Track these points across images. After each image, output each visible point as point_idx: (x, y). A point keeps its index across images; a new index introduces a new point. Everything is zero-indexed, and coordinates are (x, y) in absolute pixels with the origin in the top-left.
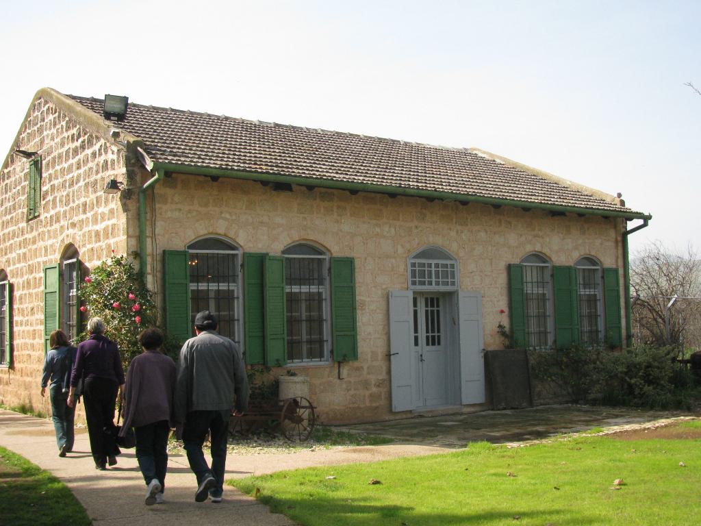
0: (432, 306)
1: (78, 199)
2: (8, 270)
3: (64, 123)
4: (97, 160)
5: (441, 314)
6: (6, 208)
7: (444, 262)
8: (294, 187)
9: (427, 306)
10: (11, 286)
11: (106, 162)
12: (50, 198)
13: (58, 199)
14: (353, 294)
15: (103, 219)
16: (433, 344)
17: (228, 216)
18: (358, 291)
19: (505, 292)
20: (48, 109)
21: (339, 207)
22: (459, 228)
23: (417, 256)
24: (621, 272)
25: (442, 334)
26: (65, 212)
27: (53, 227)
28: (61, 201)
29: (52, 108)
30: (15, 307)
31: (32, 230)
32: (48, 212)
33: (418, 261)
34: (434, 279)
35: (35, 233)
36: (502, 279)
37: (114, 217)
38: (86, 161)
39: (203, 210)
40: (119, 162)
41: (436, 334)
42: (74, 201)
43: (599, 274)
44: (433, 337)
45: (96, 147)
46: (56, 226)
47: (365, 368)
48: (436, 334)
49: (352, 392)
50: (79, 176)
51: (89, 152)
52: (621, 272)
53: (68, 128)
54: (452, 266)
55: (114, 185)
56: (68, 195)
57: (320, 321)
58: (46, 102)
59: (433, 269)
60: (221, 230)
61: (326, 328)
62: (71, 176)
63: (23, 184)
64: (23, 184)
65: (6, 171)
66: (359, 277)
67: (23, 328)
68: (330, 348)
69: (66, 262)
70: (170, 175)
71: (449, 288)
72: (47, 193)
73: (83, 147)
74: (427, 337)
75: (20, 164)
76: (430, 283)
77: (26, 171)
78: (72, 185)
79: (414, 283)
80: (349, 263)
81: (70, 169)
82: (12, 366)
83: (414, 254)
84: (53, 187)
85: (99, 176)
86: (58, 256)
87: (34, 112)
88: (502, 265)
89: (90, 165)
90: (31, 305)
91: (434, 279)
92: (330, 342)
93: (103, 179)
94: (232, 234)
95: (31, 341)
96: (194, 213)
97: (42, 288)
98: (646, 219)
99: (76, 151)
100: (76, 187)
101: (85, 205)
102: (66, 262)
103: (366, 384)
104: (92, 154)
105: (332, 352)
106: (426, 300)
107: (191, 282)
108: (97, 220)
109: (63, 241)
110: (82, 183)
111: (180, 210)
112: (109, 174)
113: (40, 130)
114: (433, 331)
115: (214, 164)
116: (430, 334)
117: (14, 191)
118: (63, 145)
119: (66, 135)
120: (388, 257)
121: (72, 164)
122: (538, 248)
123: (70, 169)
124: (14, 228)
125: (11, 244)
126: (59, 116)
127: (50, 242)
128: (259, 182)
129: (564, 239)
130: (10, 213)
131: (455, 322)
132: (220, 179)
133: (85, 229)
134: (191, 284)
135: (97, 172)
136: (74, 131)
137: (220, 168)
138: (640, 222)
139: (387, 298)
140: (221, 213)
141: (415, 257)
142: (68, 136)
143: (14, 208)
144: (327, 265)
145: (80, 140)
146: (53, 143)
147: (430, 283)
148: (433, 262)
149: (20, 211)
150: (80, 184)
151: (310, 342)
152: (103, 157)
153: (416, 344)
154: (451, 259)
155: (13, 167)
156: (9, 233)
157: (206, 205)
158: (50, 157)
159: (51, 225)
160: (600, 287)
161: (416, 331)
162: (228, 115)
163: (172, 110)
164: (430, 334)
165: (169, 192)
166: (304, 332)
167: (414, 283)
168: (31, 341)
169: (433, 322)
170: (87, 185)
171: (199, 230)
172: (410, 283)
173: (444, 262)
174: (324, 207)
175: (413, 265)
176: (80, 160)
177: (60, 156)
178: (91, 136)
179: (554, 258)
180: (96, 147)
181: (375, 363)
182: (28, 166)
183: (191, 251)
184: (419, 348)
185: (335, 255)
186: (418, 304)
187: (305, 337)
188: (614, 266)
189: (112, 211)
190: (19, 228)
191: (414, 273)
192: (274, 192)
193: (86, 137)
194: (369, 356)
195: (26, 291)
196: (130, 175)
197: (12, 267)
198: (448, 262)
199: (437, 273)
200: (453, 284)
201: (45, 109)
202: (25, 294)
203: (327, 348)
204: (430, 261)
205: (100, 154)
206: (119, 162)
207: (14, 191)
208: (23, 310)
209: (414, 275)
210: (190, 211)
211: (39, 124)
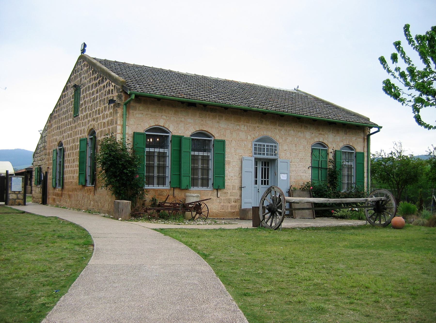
1: (96, 107)
2: (63, 141)
3: (91, 72)
4: (105, 89)
6: (63, 112)
9: (262, 166)
11: (109, 90)
12: (84, 107)
13: (87, 107)
16: (265, 184)
17: (165, 118)
20: (84, 65)
22: (280, 128)
23: (258, 141)
24: (366, 154)
25: (269, 180)
26: (90, 114)
27: (85, 121)
28: (88, 108)
29: (86, 64)
32: (82, 113)
33: (257, 143)
35: (76, 124)
37: (112, 116)
40: (114, 90)
44: (265, 181)
45: (105, 83)
46: (86, 120)
47: (229, 193)
48: (267, 167)
49: (222, 204)
50: (97, 97)
51: (102, 85)
52: (366, 154)
53: (93, 74)
54: (276, 146)
56: (92, 105)
57: (208, 170)
58: (83, 61)
59: (266, 153)
62: (93, 96)
65: (64, 94)
66: (227, 150)
67: (70, 169)
72: (82, 104)
74: (262, 181)
75: (70, 90)
76: (264, 154)
78: (93, 101)
80: (223, 142)
85: (106, 97)
95: (73, 175)
98: (380, 128)
99: (96, 85)
100: (95, 102)
101: (99, 110)
104: (103, 86)
105: (213, 184)
107: (146, 148)
110: (98, 100)
111: (142, 114)
113: (80, 75)
114: (265, 178)
116: (263, 179)
117: (67, 103)
118: (90, 82)
119: (92, 77)
121: (94, 91)
124: (67, 121)
125: (65, 129)
128: (180, 102)
129: (335, 136)
134: (146, 148)
136: (96, 75)
138: (376, 129)
140: (162, 116)
141: (256, 141)
142: (93, 78)
143: (67, 112)
145: (98, 80)
148: (266, 144)
150: (97, 101)
151: (202, 179)
155: (67, 92)
156: (64, 124)
158: (84, 88)
164: (263, 179)
167: (255, 154)
168: (73, 175)
169: (265, 174)
170: (100, 101)
172: (253, 153)
175: (255, 145)
176: (98, 89)
180: (105, 83)
181: (234, 191)
183: (147, 133)
185: (216, 138)
186: (258, 165)
188: (362, 151)
190: (69, 121)
193: (101, 78)
197: (65, 140)
198: (274, 145)
201: (83, 65)
202: (71, 153)
204: (264, 144)
206: (114, 90)
207: (67, 103)
211: (80, 71)
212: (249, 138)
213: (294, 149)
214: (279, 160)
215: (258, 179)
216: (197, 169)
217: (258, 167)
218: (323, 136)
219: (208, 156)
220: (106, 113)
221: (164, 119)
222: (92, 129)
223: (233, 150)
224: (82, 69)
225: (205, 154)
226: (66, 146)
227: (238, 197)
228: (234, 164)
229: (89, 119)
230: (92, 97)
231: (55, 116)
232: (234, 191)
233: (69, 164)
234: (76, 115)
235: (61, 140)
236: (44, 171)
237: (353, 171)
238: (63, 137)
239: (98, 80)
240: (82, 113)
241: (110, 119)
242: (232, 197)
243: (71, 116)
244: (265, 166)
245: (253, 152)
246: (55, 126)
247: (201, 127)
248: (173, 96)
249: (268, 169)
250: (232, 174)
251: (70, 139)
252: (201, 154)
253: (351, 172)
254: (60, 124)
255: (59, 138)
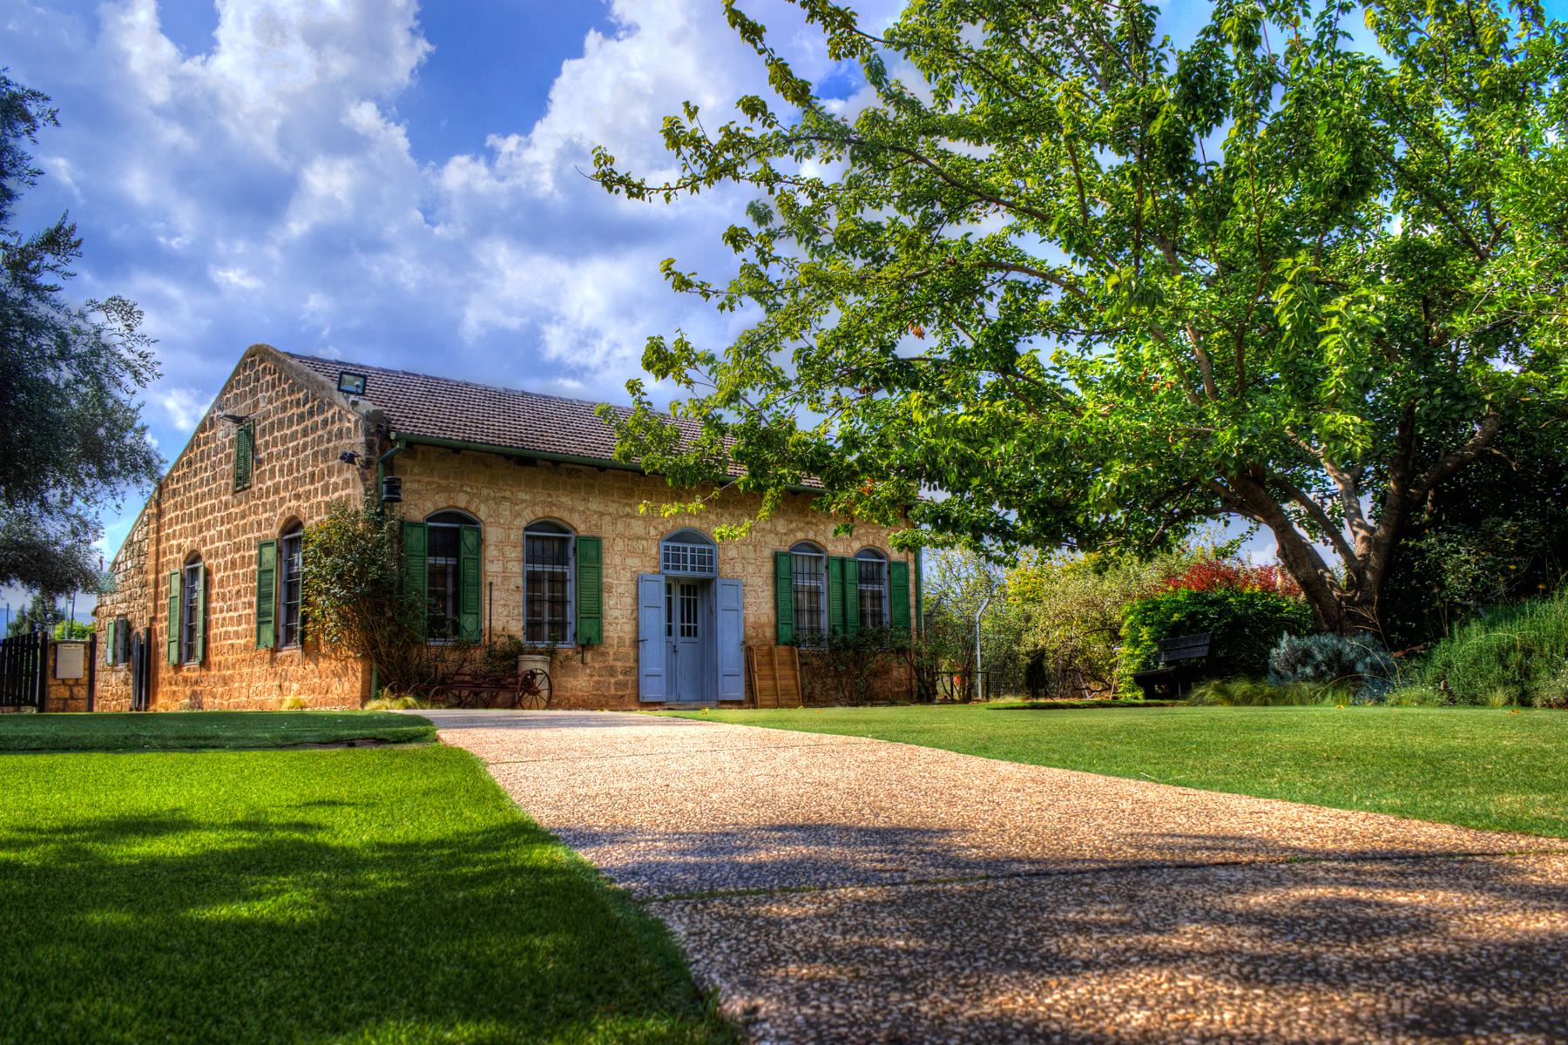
0: (689, 594)
1: (304, 469)
4: (329, 428)
5: (699, 603)
7: (702, 547)
8: (539, 462)
9: (682, 594)
10: (208, 573)
12: (266, 467)
14: (599, 577)
15: (335, 489)
16: (689, 635)
17: (469, 490)
18: (605, 572)
19: (770, 581)
20: (265, 368)
21: (587, 485)
22: (719, 510)
23: (670, 540)
24: (912, 567)
25: (699, 624)
28: (281, 470)
30: (214, 591)
31: (240, 503)
32: (263, 482)
33: (670, 544)
34: (689, 565)
36: (768, 567)
38: (314, 429)
39: (443, 482)
41: (692, 625)
42: (298, 471)
43: (885, 568)
44: (689, 628)
48: (692, 625)
49: (596, 678)
51: (319, 419)
52: (912, 567)
53: (292, 392)
54: (710, 551)
55: (349, 458)
56: (291, 464)
57: (563, 602)
58: (262, 361)
60: (462, 504)
61: (570, 610)
63: (227, 451)
64: (227, 451)
68: (573, 631)
69: (287, 537)
70: (414, 446)
71: (706, 575)
73: (311, 413)
74: (683, 627)
76: (685, 568)
77: (231, 437)
79: (667, 567)
81: (294, 436)
82: (205, 663)
83: (668, 537)
84: (270, 456)
85: (331, 445)
86: (273, 532)
87: (245, 369)
88: (767, 552)
89: (320, 432)
90: (237, 588)
91: (689, 565)
92: (573, 625)
93: (336, 448)
94: (472, 509)
96: (434, 486)
97: (254, 567)
99: (301, 418)
100: (302, 456)
101: (313, 475)
102: (287, 537)
103: (612, 671)
105: (575, 635)
106: (682, 587)
108: (328, 490)
109: (283, 514)
110: (309, 452)
112: (345, 444)
113: (253, 392)
114: (689, 621)
115: (456, 436)
116: (686, 624)
118: (284, 409)
119: (288, 398)
120: (639, 538)
121: (297, 431)
122: (811, 535)
123: (294, 436)
126: (280, 378)
127: (266, 515)
130: (208, 484)
131: (712, 612)
132: (463, 452)
133: (314, 501)
135: (329, 441)
137: (463, 440)
139: (638, 581)
141: (668, 540)
144: (571, 545)
145: (307, 406)
146: (270, 407)
147: (685, 568)
148: (689, 546)
149: (223, 482)
151: (552, 624)
152: (337, 426)
153: (669, 632)
154: (709, 544)
157: (447, 478)
159: (267, 497)
160: (886, 583)
161: (669, 619)
162: (468, 380)
163: (405, 373)
164: (686, 624)
165: (409, 463)
166: (546, 614)
167: (667, 567)
169: (690, 612)
170: (315, 455)
171: (440, 502)
173: (702, 547)
174: (944, 110)
175: (667, 548)
177: (281, 422)
178: (322, 401)
179: (830, 548)
181: (622, 650)
182: (235, 430)
184: (672, 638)
185: (581, 534)
187: (547, 618)
189: (346, 482)
191: (666, 556)
192: (517, 468)
194: (616, 641)
195: (229, 573)
196: (369, 446)
198: (706, 547)
199: (693, 558)
200: (711, 570)
203: (570, 631)
205: (333, 422)
208: (224, 595)
209: (667, 560)
210: (429, 483)
212: (653, 532)
213: (752, 555)
214: (719, 581)
215: (673, 624)
216: (542, 601)
217: (673, 596)
218: (814, 528)
219: (564, 574)
220: (332, 480)
221: (467, 493)
222: (293, 518)
223: (617, 560)
224: (257, 380)
225: (558, 569)
226: (211, 561)
227: (631, 664)
228: (621, 589)
229: (282, 494)
230: (291, 445)
231: (174, 490)
232: (622, 650)
233: (221, 604)
234: (242, 482)
235: (195, 547)
236: (140, 628)
237: (885, 603)
238: (204, 540)
239: (307, 406)
240: (263, 482)
241: (344, 493)
242: (619, 664)
243: (226, 490)
244: (689, 628)
245: (662, 564)
246: (173, 515)
247: (547, 509)
248: (488, 443)
249: (695, 600)
250: (616, 613)
251: (225, 543)
252: (548, 568)
253: (880, 606)
254: (193, 509)
255: (187, 543)
